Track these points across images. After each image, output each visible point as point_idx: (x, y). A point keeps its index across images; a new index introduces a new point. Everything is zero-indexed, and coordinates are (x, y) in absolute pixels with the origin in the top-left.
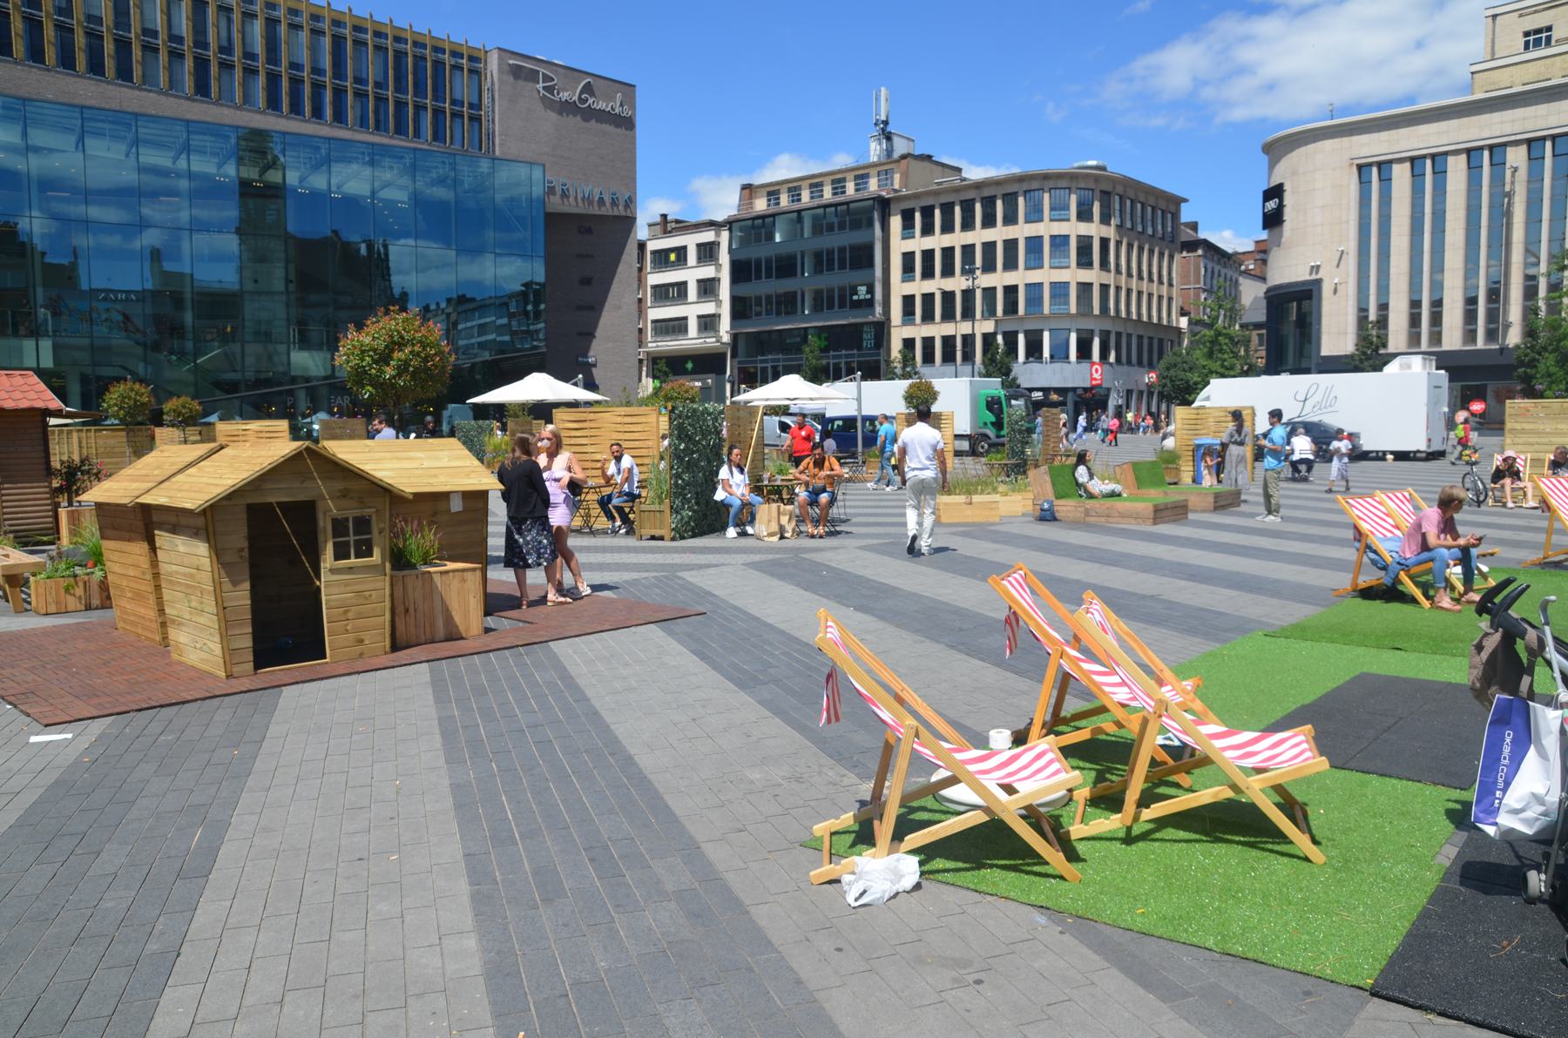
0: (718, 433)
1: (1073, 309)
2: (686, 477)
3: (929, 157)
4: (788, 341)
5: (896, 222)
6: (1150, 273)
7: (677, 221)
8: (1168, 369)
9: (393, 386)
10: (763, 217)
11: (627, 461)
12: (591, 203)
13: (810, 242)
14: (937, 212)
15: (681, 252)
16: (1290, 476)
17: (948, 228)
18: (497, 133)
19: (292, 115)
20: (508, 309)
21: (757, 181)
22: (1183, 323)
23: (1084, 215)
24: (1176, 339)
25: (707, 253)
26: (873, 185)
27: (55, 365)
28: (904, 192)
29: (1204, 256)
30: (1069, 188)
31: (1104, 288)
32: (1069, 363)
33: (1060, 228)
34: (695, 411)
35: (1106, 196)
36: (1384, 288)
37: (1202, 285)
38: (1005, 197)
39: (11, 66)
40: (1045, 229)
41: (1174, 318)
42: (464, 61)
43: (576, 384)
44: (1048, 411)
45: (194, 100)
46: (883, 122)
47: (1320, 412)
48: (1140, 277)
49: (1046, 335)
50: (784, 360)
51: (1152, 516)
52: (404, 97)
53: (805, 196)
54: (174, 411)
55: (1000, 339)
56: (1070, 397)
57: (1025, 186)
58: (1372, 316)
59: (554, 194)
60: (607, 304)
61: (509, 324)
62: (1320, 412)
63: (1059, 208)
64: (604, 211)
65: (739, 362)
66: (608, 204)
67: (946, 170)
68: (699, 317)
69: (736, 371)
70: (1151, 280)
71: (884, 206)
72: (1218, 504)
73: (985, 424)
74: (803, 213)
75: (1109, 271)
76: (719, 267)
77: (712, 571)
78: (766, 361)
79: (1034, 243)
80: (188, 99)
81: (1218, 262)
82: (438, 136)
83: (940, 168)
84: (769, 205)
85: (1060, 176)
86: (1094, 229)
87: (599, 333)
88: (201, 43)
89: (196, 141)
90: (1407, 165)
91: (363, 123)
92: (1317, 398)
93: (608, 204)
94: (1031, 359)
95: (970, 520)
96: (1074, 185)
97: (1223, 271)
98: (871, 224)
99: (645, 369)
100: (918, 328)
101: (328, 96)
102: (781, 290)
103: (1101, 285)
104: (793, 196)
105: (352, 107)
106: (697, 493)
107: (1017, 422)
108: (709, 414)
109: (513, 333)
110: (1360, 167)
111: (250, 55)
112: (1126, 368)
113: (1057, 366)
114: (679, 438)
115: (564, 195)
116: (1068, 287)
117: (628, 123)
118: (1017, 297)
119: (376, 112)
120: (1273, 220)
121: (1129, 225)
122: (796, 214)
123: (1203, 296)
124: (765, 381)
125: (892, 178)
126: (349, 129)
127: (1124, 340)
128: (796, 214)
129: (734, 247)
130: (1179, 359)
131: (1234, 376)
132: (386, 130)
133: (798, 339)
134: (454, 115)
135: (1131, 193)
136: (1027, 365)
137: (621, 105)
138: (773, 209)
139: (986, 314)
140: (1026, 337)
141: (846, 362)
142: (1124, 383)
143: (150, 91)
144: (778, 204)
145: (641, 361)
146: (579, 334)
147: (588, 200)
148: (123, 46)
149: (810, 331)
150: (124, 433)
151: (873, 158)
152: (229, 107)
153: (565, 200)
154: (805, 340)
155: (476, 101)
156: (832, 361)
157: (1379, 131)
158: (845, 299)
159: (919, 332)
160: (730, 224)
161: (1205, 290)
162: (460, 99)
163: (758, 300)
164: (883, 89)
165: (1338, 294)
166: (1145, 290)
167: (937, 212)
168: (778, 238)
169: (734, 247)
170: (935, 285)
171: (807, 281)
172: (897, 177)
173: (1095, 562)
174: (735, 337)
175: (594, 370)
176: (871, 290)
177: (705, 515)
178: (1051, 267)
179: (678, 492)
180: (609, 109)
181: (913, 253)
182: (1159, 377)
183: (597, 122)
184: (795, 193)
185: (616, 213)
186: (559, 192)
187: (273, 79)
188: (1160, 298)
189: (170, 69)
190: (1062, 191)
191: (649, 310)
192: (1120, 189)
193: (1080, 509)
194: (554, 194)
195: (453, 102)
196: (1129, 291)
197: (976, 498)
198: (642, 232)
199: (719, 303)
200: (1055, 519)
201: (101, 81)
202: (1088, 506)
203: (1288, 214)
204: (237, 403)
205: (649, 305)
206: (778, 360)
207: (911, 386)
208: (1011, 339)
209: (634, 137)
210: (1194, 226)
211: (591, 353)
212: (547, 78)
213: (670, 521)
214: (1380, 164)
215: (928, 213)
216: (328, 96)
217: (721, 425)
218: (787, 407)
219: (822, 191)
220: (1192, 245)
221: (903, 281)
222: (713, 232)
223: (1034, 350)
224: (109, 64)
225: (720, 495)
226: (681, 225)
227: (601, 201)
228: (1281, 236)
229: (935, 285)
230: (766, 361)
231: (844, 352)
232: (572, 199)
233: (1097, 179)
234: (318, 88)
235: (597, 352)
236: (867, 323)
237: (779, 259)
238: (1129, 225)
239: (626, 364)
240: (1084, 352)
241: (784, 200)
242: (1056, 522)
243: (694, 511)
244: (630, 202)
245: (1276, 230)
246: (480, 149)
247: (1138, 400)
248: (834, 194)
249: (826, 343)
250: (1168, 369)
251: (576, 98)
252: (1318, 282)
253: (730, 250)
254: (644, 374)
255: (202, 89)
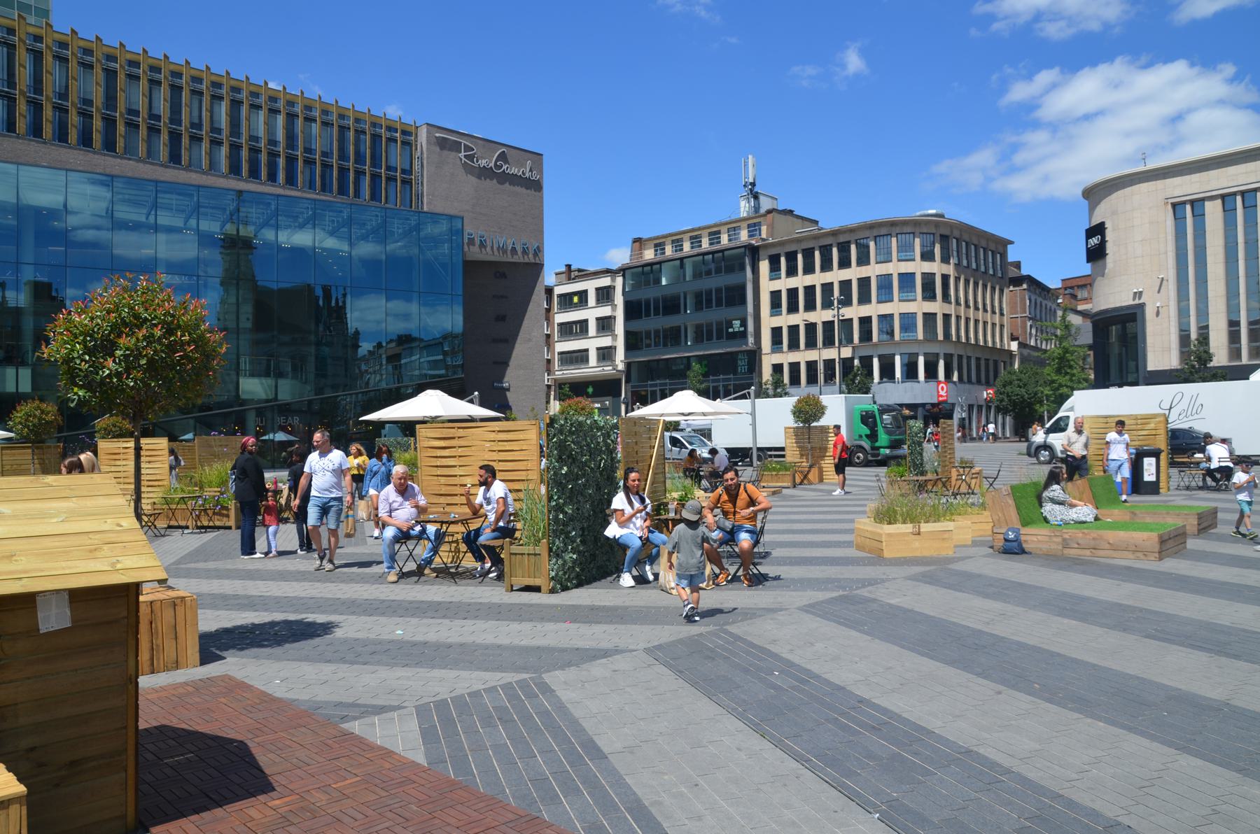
0: (611, 452)
1: (920, 336)
2: (569, 510)
3: (791, 212)
4: (674, 368)
5: (764, 266)
6: (984, 305)
7: (579, 270)
8: (1004, 386)
9: (120, 389)
10: (651, 264)
11: (498, 489)
12: (505, 252)
13: (692, 285)
14: (800, 257)
15: (583, 295)
16: (1201, 484)
17: (809, 269)
18: (425, 194)
19: (251, 179)
20: (443, 348)
21: (645, 236)
22: (1014, 346)
23: (927, 256)
24: (1008, 360)
25: (605, 295)
26: (744, 236)
27: (32, 389)
28: (771, 240)
29: (1028, 290)
30: (913, 233)
31: (947, 317)
32: (919, 382)
33: (906, 267)
34: (580, 424)
35: (944, 239)
36: (1203, 313)
37: (1027, 314)
38: (858, 246)
39: (14, 139)
40: (894, 268)
41: (1006, 342)
42: (398, 135)
43: (471, 401)
44: (944, 423)
45: (167, 167)
46: (751, 184)
47: (1185, 419)
48: (977, 309)
49: (898, 359)
50: (671, 384)
51: (1157, 549)
52: (347, 164)
53: (687, 247)
54: (105, 429)
55: (856, 362)
56: (920, 411)
57: (875, 232)
58: (1194, 336)
59: (474, 244)
60: (519, 337)
61: (444, 360)
62: (1185, 419)
63: (906, 249)
64: (515, 259)
65: (633, 387)
66: (519, 253)
67: (805, 222)
68: (598, 349)
69: (630, 394)
70: (985, 310)
71: (754, 252)
72: (1201, 527)
73: (861, 436)
74: (685, 260)
75: (950, 303)
76: (614, 307)
77: (598, 669)
78: (655, 385)
79: (885, 281)
80: (162, 165)
81: (1040, 295)
82: (375, 196)
83: (800, 221)
84: (656, 255)
85: (905, 223)
86: (936, 267)
87: (512, 363)
88: (175, 117)
89: (164, 199)
90: (1219, 202)
91: (312, 186)
92: (1184, 405)
93: (519, 253)
94: (885, 380)
95: (918, 554)
96: (917, 231)
97: (1044, 302)
98: (743, 268)
99: (552, 393)
100: (785, 354)
101: (281, 162)
102: (668, 326)
103: (944, 315)
104: (676, 247)
105: (302, 173)
106: (583, 529)
107: (916, 434)
108: (600, 429)
109: (447, 368)
110: (1174, 205)
111: (215, 130)
112: (967, 386)
113: (909, 385)
114: (560, 459)
115: (482, 245)
116: (916, 317)
117: (536, 186)
118: (871, 327)
119: (323, 177)
120: (1096, 254)
121: (965, 263)
122: (678, 262)
123: (1029, 324)
124: (654, 401)
125: (760, 230)
126: (299, 190)
127: (965, 361)
128: (678, 262)
129: (627, 290)
130: (1015, 378)
131: (1083, 389)
132: (331, 191)
133: (682, 367)
134: (389, 179)
135: (966, 237)
136: (881, 385)
137: (531, 170)
138: (659, 258)
139: (844, 342)
140: (880, 361)
141: (660, 390)
142: (966, 399)
143: (130, 159)
144: (664, 253)
145: (549, 387)
146: (495, 363)
147: (502, 250)
148: (110, 122)
149: (692, 359)
150: (30, 451)
151: (743, 214)
152: (196, 172)
153: (483, 250)
154: (689, 367)
155: (408, 168)
156: (711, 385)
157: (1190, 173)
158: (722, 332)
159: (786, 358)
160: (623, 271)
161: (1030, 319)
162: (394, 166)
163: (648, 334)
164: (750, 157)
165: (1160, 317)
166: (980, 319)
167: (800, 257)
168: (664, 282)
169: (627, 290)
170: (799, 319)
171: (689, 318)
172: (764, 229)
173: (1200, 648)
174: (629, 366)
175: (508, 394)
176: (744, 323)
177: (593, 556)
178: (900, 301)
179: (558, 529)
180: (521, 173)
181: (780, 291)
182: (998, 392)
183: (510, 184)
184: (678, 244)
185: (526, 260)
186: (477, 242)
187: (235, 148)
188: (994, 325)
189: (149, 141)
190: (907, 235)
191: (556, 344)
192: (956, 233)
193: (1055, 539)
194: (474, 244)
195: (388, 168)
196: (967, 320)
197: (926, 527)
198: (549, 278)
199: (615, 337)
200: (1023, 552)
201: (89, 151)
202: (1066, 536)
203: (1110, 248)
204: (192, 422)
205: (556, 339)
206: (665, 384)
207: (799, 401)
208: (867, 362)
209: (542, 198)
210: (1018, 265)
211: (506, 379)
212: (468, 148)
213: (546, 569)
214: (1192, 202)
215: (791, 257)
216: (281, 162)
217: (615, 442)
218: (677, 423)
219: (701, 241)
220: (1017, 281)
221: (771, 316)
222: (609, 278)
223: (887, 372)
224: (97, 138)
225: (613, 531)
226: (583, 273)
227: (514, 250)
228: (1104, 267)
229: (799, 319)
230: (655, 385)
231: (721, 377)
232: (488, 249)
233: (937, 224)
234: (273, 155)
235: (513, 378)
236: (741, 352)
237: (665, 299)
238: (965, 263)
239: (535, 388)
240: (931, 373)
241: (669, 251)
242: (1024, 556)
243: (579, 553)
244: (538, 251)
245: (1100, 263)
246: (411, 207)
247: (978, 413)
248: (711, 244)
249: (706, 369)
250: (1004, 386)
251: (492, 165)
252: (1142, 306)
253: (624, 293)
254: (552, 397)
255: (175, 158)
